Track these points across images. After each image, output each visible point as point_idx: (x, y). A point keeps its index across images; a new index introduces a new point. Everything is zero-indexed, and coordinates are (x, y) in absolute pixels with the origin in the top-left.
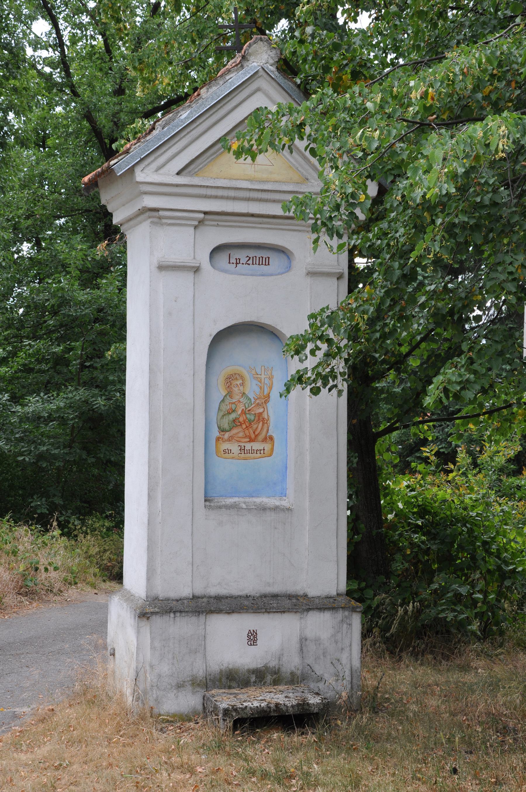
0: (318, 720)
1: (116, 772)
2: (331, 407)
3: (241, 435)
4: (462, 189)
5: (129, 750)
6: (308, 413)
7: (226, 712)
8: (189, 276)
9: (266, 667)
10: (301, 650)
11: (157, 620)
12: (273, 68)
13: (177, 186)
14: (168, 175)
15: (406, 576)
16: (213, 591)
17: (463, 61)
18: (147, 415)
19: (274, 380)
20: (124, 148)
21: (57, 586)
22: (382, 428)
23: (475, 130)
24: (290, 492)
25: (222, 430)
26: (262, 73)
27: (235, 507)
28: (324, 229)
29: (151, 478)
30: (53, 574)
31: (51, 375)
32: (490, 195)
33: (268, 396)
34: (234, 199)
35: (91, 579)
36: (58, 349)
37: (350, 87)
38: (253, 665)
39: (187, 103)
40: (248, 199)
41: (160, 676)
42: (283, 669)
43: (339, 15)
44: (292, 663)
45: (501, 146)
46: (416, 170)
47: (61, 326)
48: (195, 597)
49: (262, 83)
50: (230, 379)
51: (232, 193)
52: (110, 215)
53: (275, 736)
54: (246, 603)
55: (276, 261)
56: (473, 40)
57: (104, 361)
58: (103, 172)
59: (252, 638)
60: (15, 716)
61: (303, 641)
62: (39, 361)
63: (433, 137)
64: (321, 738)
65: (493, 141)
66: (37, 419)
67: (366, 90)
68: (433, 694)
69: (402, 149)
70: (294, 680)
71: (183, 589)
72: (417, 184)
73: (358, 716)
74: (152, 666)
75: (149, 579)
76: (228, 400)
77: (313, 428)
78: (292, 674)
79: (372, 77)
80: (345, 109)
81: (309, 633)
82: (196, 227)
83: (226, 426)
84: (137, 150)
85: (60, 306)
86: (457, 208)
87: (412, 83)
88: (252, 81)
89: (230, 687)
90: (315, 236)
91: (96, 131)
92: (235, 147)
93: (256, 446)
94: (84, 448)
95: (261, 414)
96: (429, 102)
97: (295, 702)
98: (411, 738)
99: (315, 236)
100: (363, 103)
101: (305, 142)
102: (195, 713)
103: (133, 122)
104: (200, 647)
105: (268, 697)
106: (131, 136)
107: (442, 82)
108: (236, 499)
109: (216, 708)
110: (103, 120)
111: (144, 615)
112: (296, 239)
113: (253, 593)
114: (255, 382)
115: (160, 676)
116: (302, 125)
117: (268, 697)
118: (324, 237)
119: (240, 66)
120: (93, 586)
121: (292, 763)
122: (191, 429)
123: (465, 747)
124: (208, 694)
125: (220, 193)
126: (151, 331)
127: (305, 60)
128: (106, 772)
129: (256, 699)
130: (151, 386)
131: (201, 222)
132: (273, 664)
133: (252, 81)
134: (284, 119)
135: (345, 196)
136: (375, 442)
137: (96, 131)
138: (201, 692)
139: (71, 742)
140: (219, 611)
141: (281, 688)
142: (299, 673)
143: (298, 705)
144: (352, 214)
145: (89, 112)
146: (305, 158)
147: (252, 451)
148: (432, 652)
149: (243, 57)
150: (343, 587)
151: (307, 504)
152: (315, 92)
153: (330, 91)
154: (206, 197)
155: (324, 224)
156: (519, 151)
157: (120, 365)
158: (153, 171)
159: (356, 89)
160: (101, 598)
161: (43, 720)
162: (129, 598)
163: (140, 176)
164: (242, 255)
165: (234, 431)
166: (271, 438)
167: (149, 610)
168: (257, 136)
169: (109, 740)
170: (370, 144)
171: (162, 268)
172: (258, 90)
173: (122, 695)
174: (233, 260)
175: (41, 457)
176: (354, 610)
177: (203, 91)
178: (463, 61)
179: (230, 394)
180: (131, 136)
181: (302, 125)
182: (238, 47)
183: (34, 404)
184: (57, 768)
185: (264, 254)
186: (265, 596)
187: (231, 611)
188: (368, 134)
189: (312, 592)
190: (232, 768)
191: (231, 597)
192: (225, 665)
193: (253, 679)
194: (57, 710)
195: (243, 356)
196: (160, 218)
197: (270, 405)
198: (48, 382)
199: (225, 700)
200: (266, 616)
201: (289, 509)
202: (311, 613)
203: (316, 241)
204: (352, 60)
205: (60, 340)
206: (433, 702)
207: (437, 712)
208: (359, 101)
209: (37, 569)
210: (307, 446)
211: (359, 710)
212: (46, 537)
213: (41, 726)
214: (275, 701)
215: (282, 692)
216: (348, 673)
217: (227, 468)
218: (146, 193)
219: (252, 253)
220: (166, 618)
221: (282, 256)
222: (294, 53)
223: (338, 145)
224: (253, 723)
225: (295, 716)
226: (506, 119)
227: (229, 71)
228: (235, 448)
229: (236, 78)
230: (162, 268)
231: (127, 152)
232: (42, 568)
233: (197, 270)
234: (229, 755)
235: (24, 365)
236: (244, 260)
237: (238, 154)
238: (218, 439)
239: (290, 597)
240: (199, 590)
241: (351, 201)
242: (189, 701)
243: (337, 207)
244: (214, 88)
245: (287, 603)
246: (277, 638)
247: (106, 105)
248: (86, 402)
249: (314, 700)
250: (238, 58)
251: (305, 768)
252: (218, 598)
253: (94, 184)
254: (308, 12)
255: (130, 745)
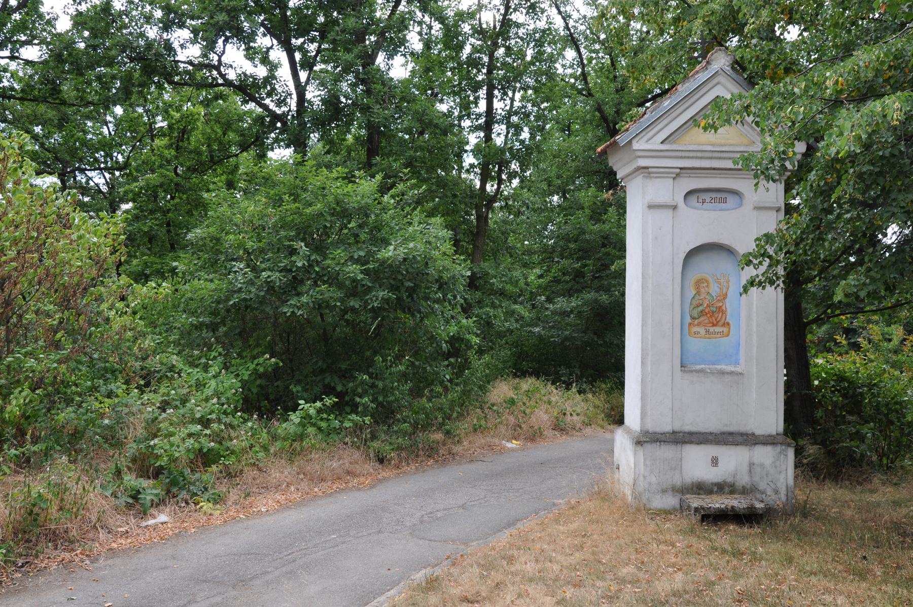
0: (762, 519)
1: (622, 542)
2: (771, 302)
3: (706, 321)
4: (867, 146)
5: (631, 529)
6: (755, 306)
7: (696, 510)
8: (670, 212)
9: (725, 482)
10: (750, 471)
11: (648, 447)
12: (729, 68)
13: (661, 151)
14: (655, 144)
15: (827, 424)
16: (687, 428)
17: (865, 58)
18: (641, 308)
19: (731, 284)
20: (625, 128)
21: (578, 425)
22: (811, 318)
23: (875, 106)
24: (742, 361)
25: (693, 318)
26: (721, 72)
27: (702, 371)
28: (762, 177)
29: (643, 350)
30: (575, 418)
31: (575, 282)
32: (889, 150)
33: (726, 294)
34: (701, 158)
35: (601, 422)
36: (577, 265)
37: (783, 79)
38: (715, 480)
39: (668, 95)
40: (711, 158)
41: (650, 484)
42: (737, 484)
43: (776, 28)
44: (743, 480)
45: (895, 117)
46: (831, 135)
47: (579, 250)
48: (674, 432)
49: (721, 79)
50: (698, 283)
51: (699, 154)
52: (615, 174)
53: (731, 527)
54: (710, 437)
55: (731, 200)
56: (876, 40)
57: (609, 272)
58: (611, 144)
59: (715, 461)
60: (554, 505)
61: (751, 465)
62: (564, 274)
63: (844, 112)
64: (764, 531)
65: (890, 113)
66: (565, 314)
67: (795, 80)
68: (849, 507)
69: (820, 119)
70: (744, 491)
71: (666, 426)
72: (831, 144)
73: (792, 518)
74: (644, 477)
75: (642, 419)
76: (697, 297)
77: (760, 315)
78: (743, 487)
79: (800, 71)
80: (780, 94)
81: (756, 460)
82: (674, 179)
83: (696, 315)
84: (634, 128)
85: (579, 234)
86: (864, 160)
87: (828, 74)
88: (715, 81)
89: (699, 494)
90: (756, 181)
91: (604, 118)
92: (702, 124)
93: (717, 329)
94: (595, 334)
95: (720, 307)
96: (839, 87)
97: (745, 506)
98: (832, 535)
99: (756, 181)
100: (793, 90)
101: (751, 118)
102: (675, 509)
103: (630, 110)
104: (678, 465)
105: (726, 501)
106: (628, 120)
107: (849, 73)
108: (703, 366)
109: (689, 506)
110: (609, 111)
111: (639, 443)
112: (744, 185)
113: (715, 431)
114: (716, 285)
115: (650, 484)
116: (748, 106)
117: (726, 501)
118: (763, 182)
119: (705, 68)
120: (602, 427)
121: (743, 545)
122: (671, 317)
123: (873, 543)
124: (684, 498)
125: (691, 154)
126: (643, 250)
127: (750, 62)
128: (615, 542)
129: (718, 503)
130: (644, 287)
131: (678, 175)
132: (730, 480)
133: (715, 81)
134: (737, 103)
135: (778, 153)
136: (805, 328)
137: (604, 118)
138: (679, 496)
139: (592, 522)
140: (691, 442)
141: (735, 496)
142: (748, 487)
143: (748, 508)
144: (783, 165)
145: (599, 105)
146: (752, 128)
147: (714, 333)
148: (848, 479)
149: (708, 62)
150: (781, 427)
151: (755, 370)
152: (758, 84)
153: (769, 83)
154: (681, 157)
155: (763, 173)
156: (909, 118)
157: (621, 275)
158: (646, 141)
159: (788, 80)
160: (608, 436)
161: (572, 508)
162: (629, 431)
163: (636, 146)
164: (707, 197)
165: (702, 319)
166: (728, 324)
167: (642, 439)
168: (718, 114)
169: (617, 522)
170: (797, 117)
171: (651, 207)
172: (718, 83)
173: (624, 494)
174: (700, 200)
175: (566, 339)
176: (789, 445)
177: (679, 87)
178: (865, 58)
179: (698, 293)
180: (628, 120)
181: (748, 106)
182: (704, 56)
183: (561, 303)
184: (583, 536)
185: (723, 195)
186: (724, 433)
187: (700, 443)
188: (795, 110)
189: (759, 432)
190: (702, 546)
191: (700, 433)
192: (696, 479)
193: (715, 489)
194: (582, 502)
195: (706, 266)
196: (649, 173)
197: (727, 301)
198: (571, 289)
199: (695, 502)
200: (725, 447)
201: (741, 374)
202: (757, 446)
203: (756, 184)
204: (784, 60)
205: (578, 259)
206: (849, 513)
207: (852, 519)
208: (790, 88)
209: (565, 414)
210: (755, 329)
211: (793, 514)
212: (569, 393)
213: (572, 512)
214: (731, 504)
215: (736, 499)
216: (784, 488)
217: (696, 345)
218: (640, 157)
219: (714, 195)
220: (654, 445)
221: (737, 197)
222: (742, 57)
223: (775, 120)
224: (716, 518)
225: (744, 515)
226: (899, 97)
227: (697, 72)
228: (702, 330)
229: (702, 77)
230: (651, 207)
231: (627, 130)
232: (568, 413)
233: (675, 208)
234: (699, 537)
235: (555, 277)
236: (708, 200)
237: (705, 129)
238: (690, 324)
239: (742, 434)
240: (677, 428)
241: (783, 156)
242: (671, 501)
243: (772, 161)
244: (687, 84)
245: (740, 439)
246: (732, 463)
247: (609, 98)
248: (596, 299)
249: (759, 505)
250: (704, 63)
251: (753, 549)
252: (691, 434)
253: (604, 152)
254: (754, 29)
255: (632, 526)
